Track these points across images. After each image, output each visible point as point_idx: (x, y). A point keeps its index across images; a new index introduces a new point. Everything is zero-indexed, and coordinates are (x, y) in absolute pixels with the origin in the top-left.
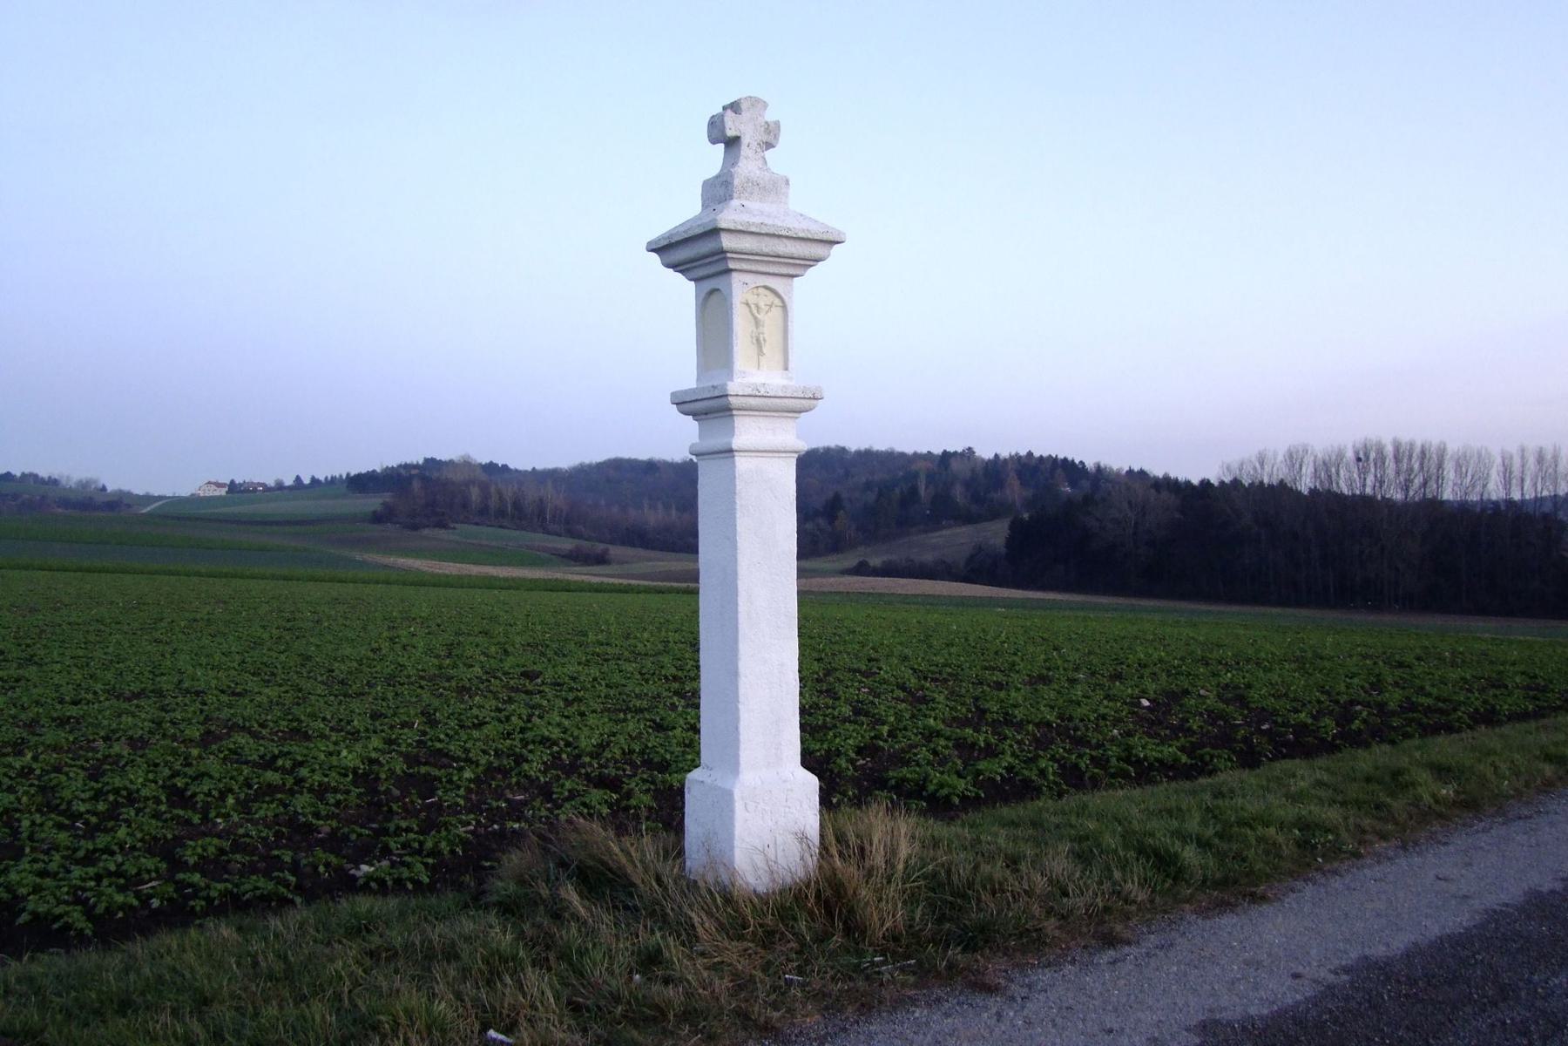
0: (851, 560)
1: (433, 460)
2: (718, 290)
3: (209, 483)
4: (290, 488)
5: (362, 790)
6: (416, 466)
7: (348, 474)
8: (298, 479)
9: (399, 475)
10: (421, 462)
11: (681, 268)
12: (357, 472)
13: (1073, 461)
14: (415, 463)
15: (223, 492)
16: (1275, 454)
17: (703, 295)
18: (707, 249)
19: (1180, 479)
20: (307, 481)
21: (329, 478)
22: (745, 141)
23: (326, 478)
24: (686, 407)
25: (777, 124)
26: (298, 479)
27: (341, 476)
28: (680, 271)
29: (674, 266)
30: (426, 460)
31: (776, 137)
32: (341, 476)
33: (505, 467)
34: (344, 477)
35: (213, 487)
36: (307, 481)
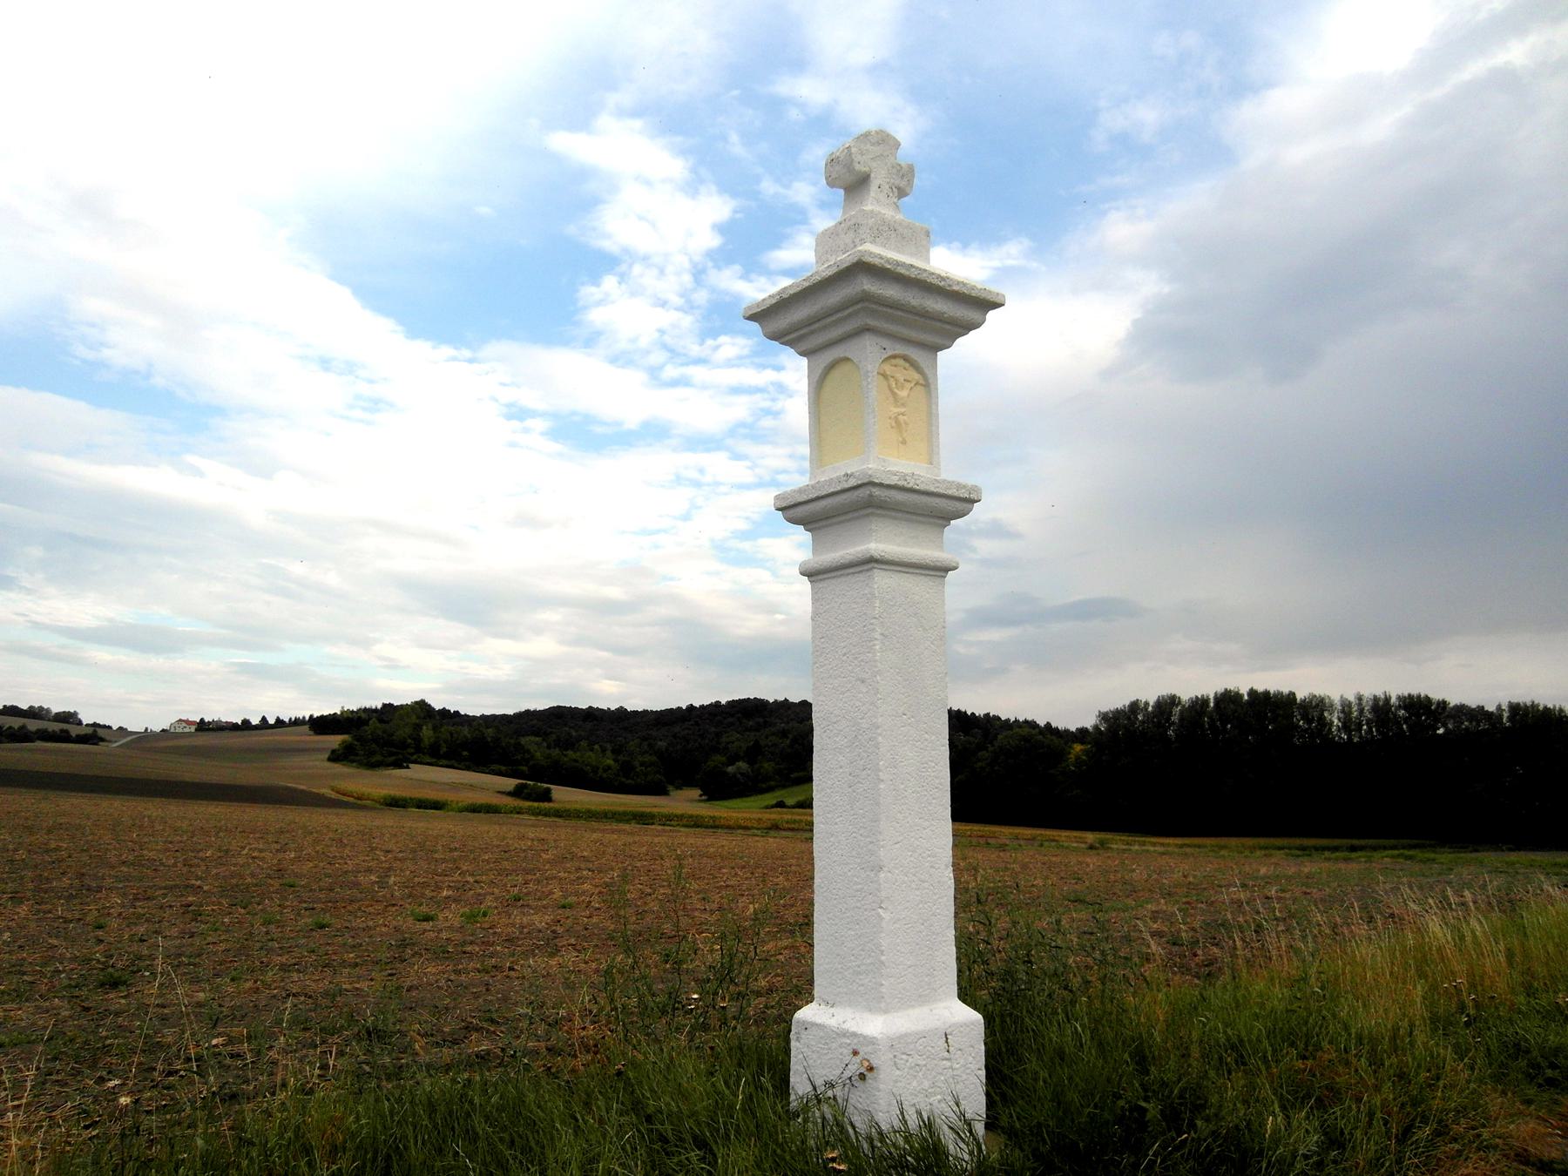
0: (770, 798)
1: (391, 705)
2: (847, 359)
3: (180, 720)
4: (256, 727)
5: (1150, 709)
6: (376, 710)
7: (311, 716)
8: (264, 719)
9: (360, 718)
10: (379, 707)
11: (787, 338)
12: (319, 715)
13: (966, 712)
14: (374, 707)
15: (193, 729)
16: (1147, 704)
17: (819, 371)
18: (838, 299)
19: (1060, 728)
20: (272, 721)
21: (293, 719)
22: (875, 183)
23: (290, 719)
24: (792, 512)
25: (911, 169)
26: (264, 719)
27: (304, 718)
28: (790, 344)
29: (776, 336)
30: (385, 705)
31: (910, 182)
32: (304, 718)
33: (457, 713)
34: (307, 718)
35: (184, 725)
36: (272, 721)
